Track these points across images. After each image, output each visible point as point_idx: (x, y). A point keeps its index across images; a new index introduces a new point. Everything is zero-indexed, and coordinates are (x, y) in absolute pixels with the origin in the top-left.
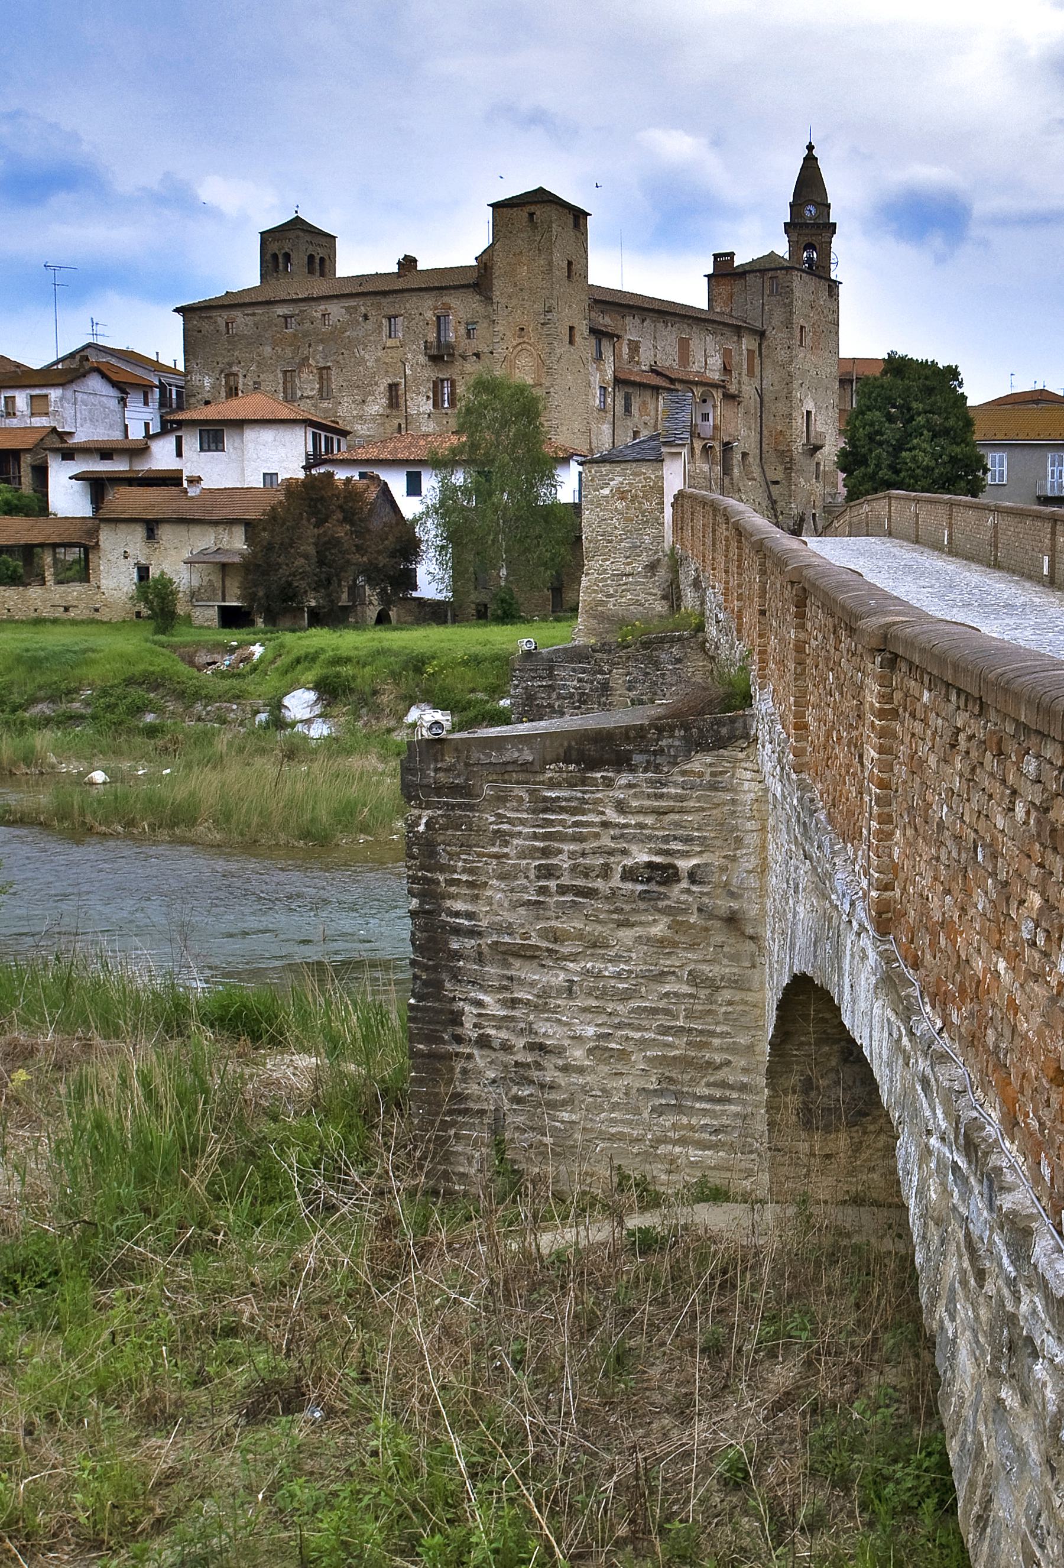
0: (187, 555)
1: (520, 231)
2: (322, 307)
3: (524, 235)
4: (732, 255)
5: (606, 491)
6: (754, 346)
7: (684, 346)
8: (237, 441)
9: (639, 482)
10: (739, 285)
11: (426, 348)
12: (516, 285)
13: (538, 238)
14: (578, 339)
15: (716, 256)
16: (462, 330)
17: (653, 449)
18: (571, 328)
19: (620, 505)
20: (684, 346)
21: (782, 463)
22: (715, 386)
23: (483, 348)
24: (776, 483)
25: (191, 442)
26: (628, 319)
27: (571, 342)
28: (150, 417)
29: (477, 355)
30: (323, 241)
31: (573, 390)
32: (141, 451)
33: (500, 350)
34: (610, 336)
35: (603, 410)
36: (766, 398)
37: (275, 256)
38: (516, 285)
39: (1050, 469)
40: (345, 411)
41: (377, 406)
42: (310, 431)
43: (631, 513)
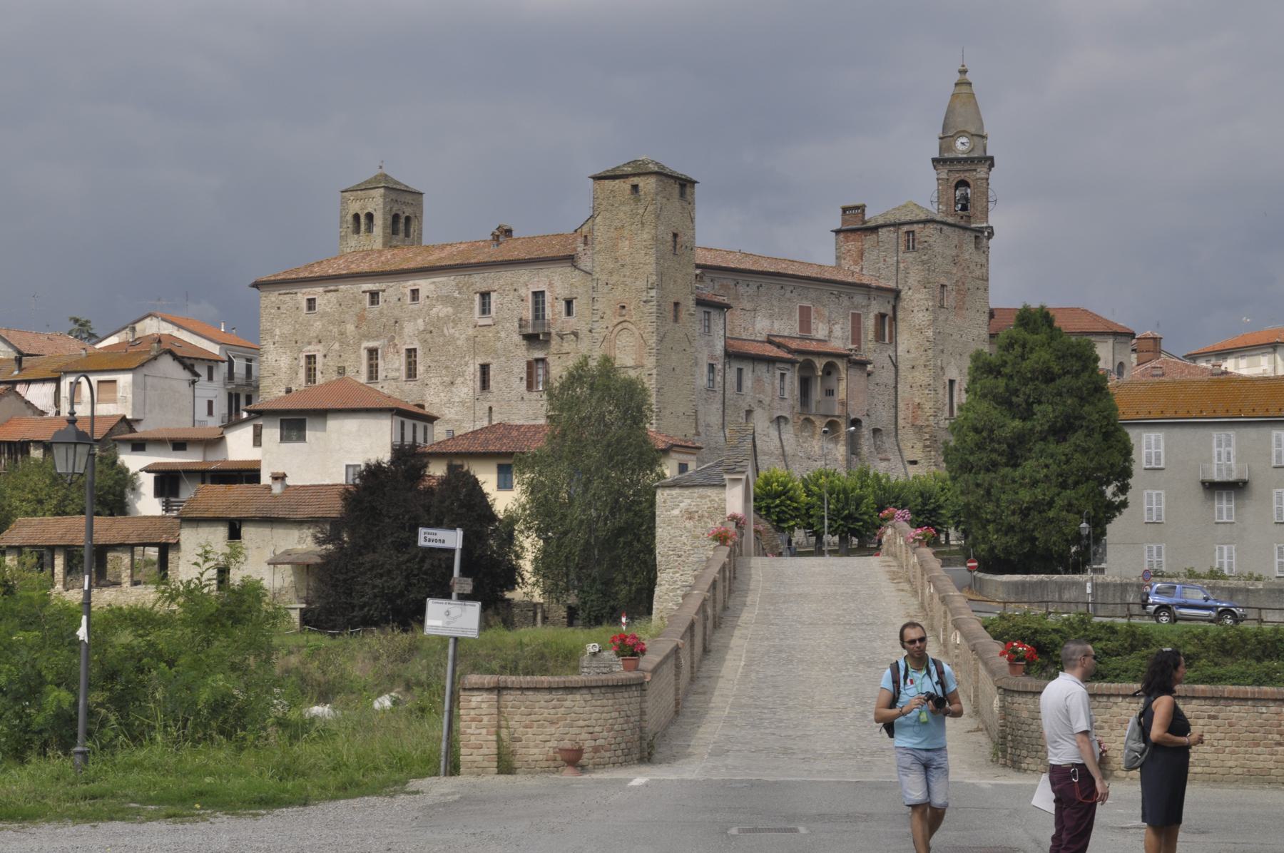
0: (269, 555)
1: (623, 203)
2: (411, 283)
3: (626, 208)
4: (862, 208)
5: (676, 512)
6: (887, 309)
7: (805, 315)
8: (319, 434)
9: (705, 504)
10: (870, 240)
11: (520, 326)
12: (617, 260)
13: (641, 211)
14: (683, 314)
15: (845, 210)
16: (562, 306)
17: (718, 474)
18: (676, 304)
19: (689, 524)
20: (805, 315)
21: (920, 440)
22: (841, 356)
23: (583, 328)
24: (914, 463)
25: (272, 433)
26: (742, 289)
27: (676, 319)
28: (216, 393)
29: (575, 334)
30: (409, 198)
31: (677, 371)
32: (216, 442)
33: (600, 329)
34: (722, 307)
35: (710, 389)
36: (901, 366)
37: (356, 217)
38: (617, 260)
39: (1215, 450)
40: (434, 400)
41: (467, 388)
42: (399, 419)
43: (698, 531)
